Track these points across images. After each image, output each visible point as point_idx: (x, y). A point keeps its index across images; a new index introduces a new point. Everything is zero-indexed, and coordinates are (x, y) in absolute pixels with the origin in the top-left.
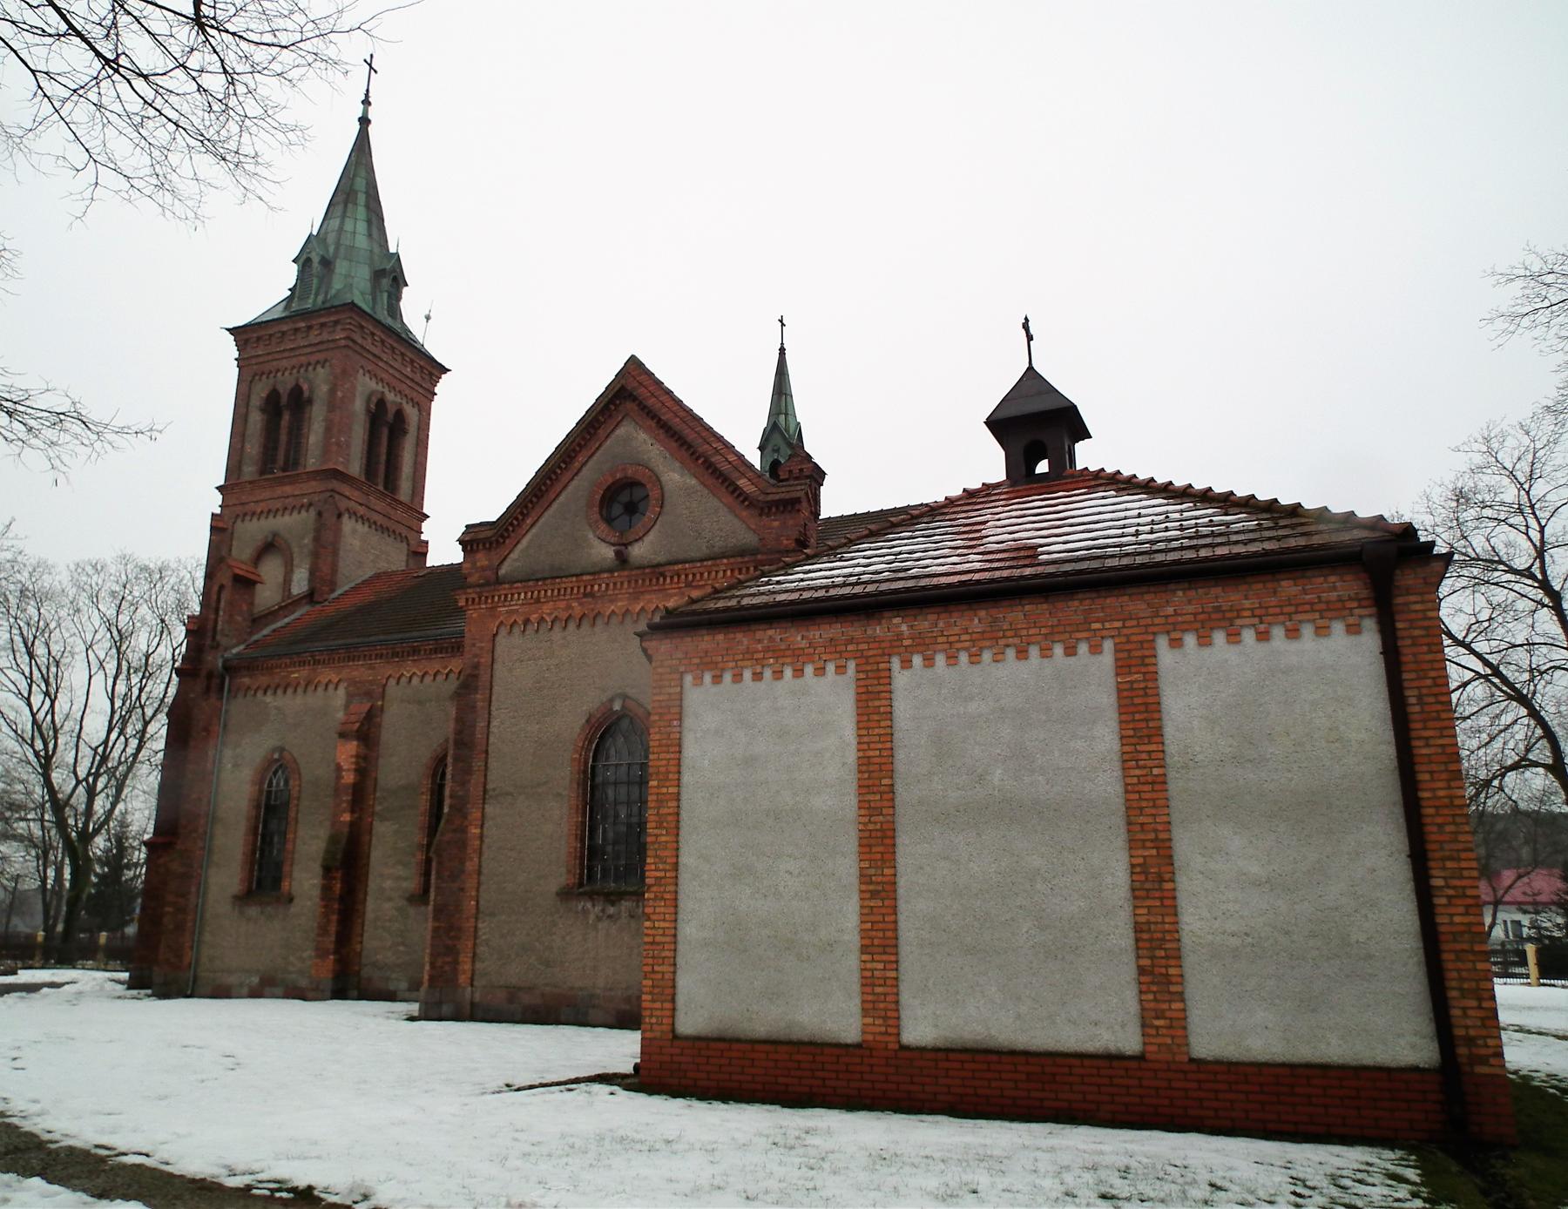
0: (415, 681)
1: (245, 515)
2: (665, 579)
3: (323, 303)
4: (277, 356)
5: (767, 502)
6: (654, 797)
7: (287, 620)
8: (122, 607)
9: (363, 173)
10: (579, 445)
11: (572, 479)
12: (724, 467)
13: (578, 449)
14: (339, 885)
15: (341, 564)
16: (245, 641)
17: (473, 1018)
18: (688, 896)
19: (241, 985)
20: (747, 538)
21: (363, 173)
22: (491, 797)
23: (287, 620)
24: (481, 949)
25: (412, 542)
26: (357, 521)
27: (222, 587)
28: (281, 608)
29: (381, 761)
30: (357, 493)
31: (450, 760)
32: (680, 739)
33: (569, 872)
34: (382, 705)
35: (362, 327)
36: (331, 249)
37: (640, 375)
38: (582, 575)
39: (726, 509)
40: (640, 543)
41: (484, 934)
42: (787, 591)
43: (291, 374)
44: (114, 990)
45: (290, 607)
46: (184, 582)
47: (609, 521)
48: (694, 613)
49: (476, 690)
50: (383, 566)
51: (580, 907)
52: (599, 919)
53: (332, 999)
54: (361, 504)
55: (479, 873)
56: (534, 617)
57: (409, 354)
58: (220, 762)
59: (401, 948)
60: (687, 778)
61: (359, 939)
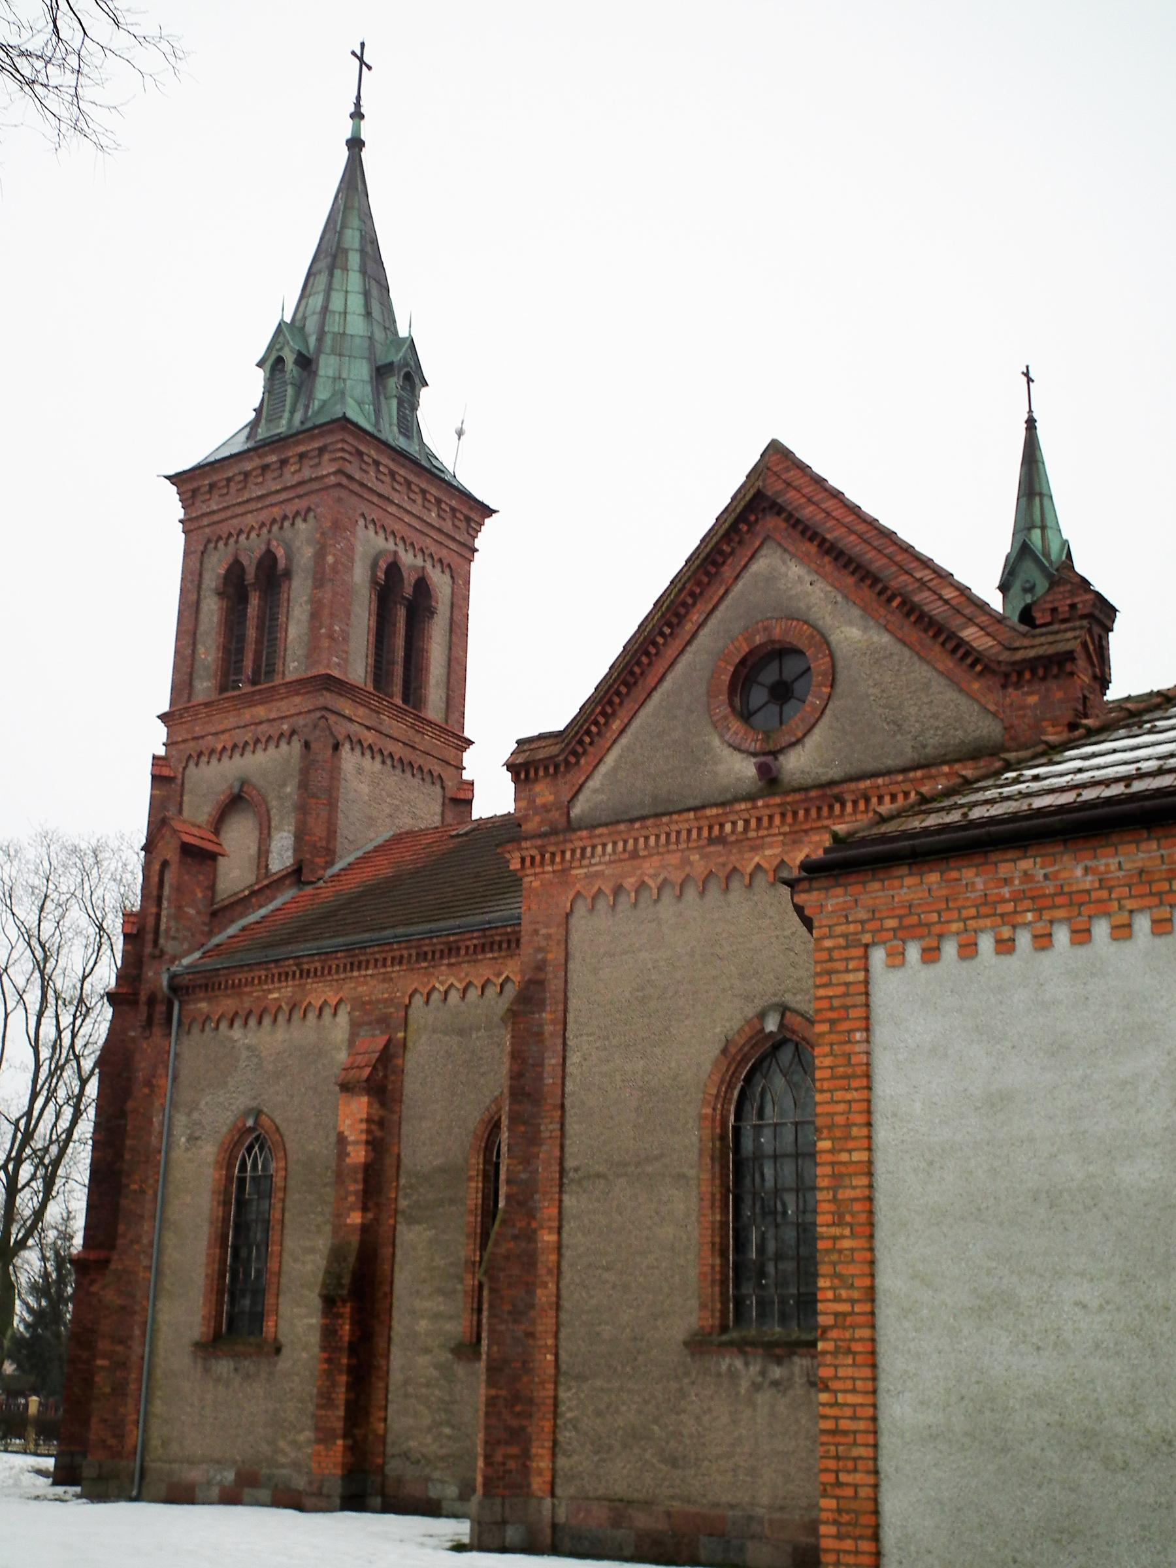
0: (454, 997)
1: (200, 754)
2: (843, 805)
3: (302, 423)
4: (239, 510)
5: (1014, 663)
6: (827, 1170)
7: (263, 911)
8: (46, 910)
9: (355, 222)
10: (692, 594)
11: (682, 652)
12: (936, 609)
13: (690, 601)
14: (347, 1327)
15: (342, 822)
16: (203, 945)
17: (555, 1550)
18: (896, 1349)
19: (209, 1483)
20: (987, 729)
21: (355, 222)
22: (572, 1180)
23: (263, 911)
24: (565, 1436)
25: (449, 784)
26: (363, 754)
27: (165, 864)
28: (253, 893)
29: (406, 1128)
30: (362, 711)
31: (505, 1122)
32: (868, 1064)
33: (703, 1306)
34: (405, 1038)
35: (360, 454)
36: (312, 341)
37: (787, 469)
38: (703, 807)
39: (943, 681)
40: (799, 748)
41: (570, 1409)
42: (1052, 791)
43: (258, 535)
44: (34, 1485)
45: (268, 892)
46: (130, 868)
47: (746, 716)
48: (884, 839)
49: (541, 1005)
50: (406, 823)
51: (724, 1367)
52: (756, 1387)
53: (343, 1508)
54: (369, 728)
55: (558, 1307)
56: (630, 882)
57: (433, 491)
58: (170, 1135)
59: (447, 1431)
60: (883, 1134)
61: (381, 1414)
